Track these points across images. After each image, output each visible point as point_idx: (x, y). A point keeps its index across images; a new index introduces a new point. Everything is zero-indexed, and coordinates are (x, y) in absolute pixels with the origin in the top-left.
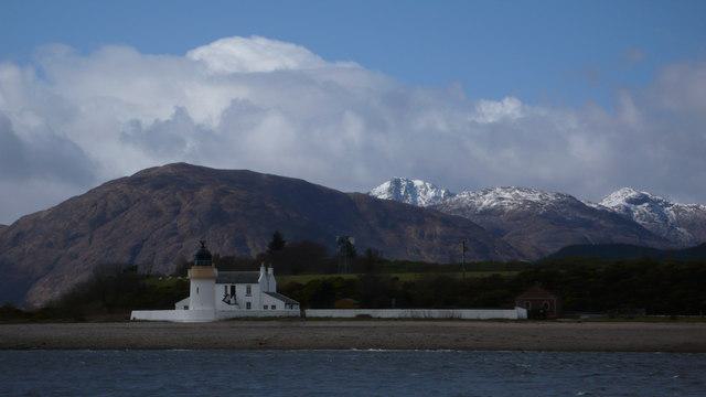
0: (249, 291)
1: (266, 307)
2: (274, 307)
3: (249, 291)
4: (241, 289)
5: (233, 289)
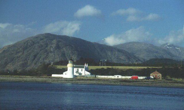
0: (82, 70)
3: (82, 70)
4: (80, 69)
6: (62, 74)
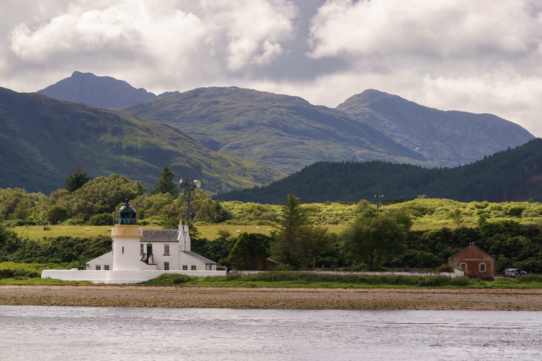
1: (185, 268)
5: (150, 248)
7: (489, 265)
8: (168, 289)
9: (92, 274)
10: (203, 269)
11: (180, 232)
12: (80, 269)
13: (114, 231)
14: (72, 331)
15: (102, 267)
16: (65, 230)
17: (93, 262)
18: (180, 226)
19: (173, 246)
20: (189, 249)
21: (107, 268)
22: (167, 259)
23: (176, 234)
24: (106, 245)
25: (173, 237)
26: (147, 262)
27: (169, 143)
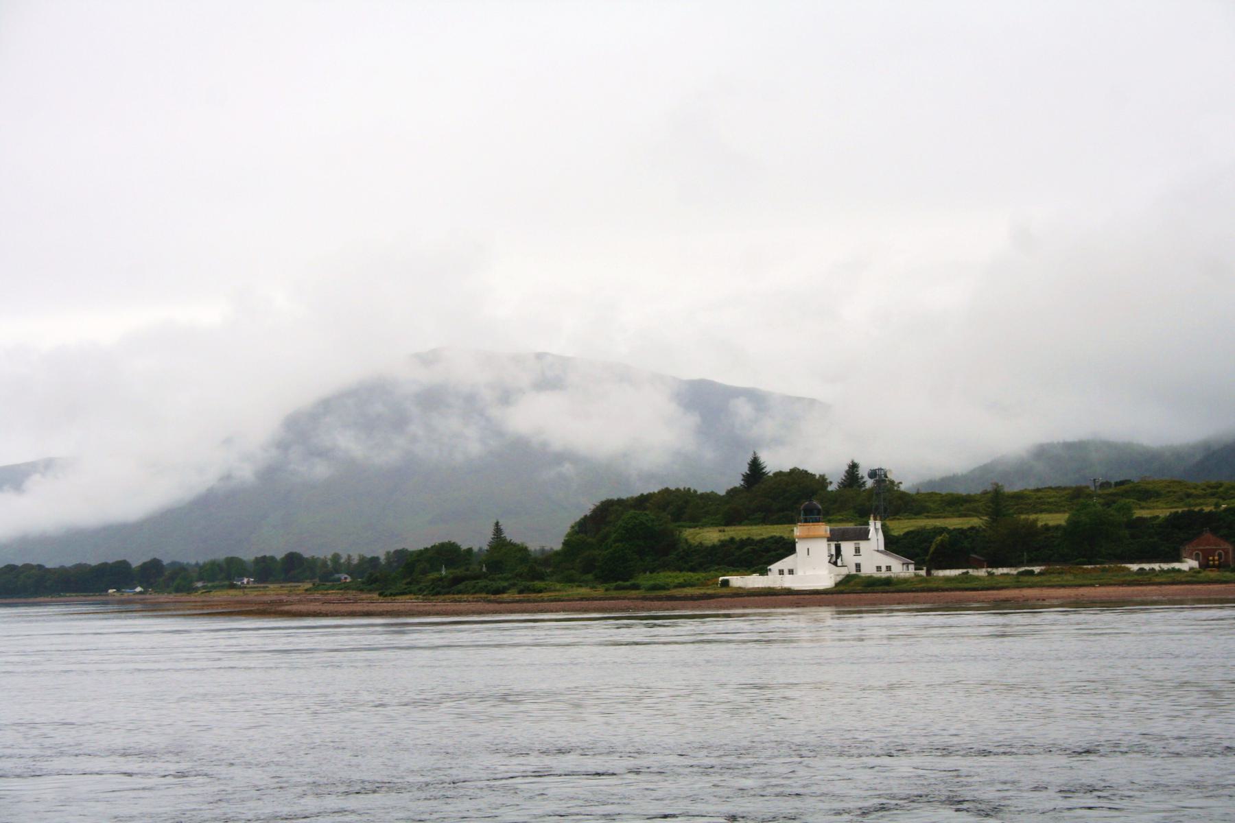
0: (857, 551)
1: (879, 568)
2: (889, 568)
3: (857, 551)
5: (838, 549)
6: (764, 572)
7: (1227, 553)
8: (855, 593)
9: (773, 579)
10: (898, 568)
11: (872, 528)
12: (762, 574)
13: (798, 530)
14: (850, 622)
15: (786, 572)
16: (740, 532)
17: (775, 567)
18: (871, 522)
19: (863, 545)
20: (882, 547)
21: (791, 572)
22: (858, 560)
23: (867, 532)
24: (788, 548)
25: (864, 536)
26: (835, 564)
27: (1019, 782)
